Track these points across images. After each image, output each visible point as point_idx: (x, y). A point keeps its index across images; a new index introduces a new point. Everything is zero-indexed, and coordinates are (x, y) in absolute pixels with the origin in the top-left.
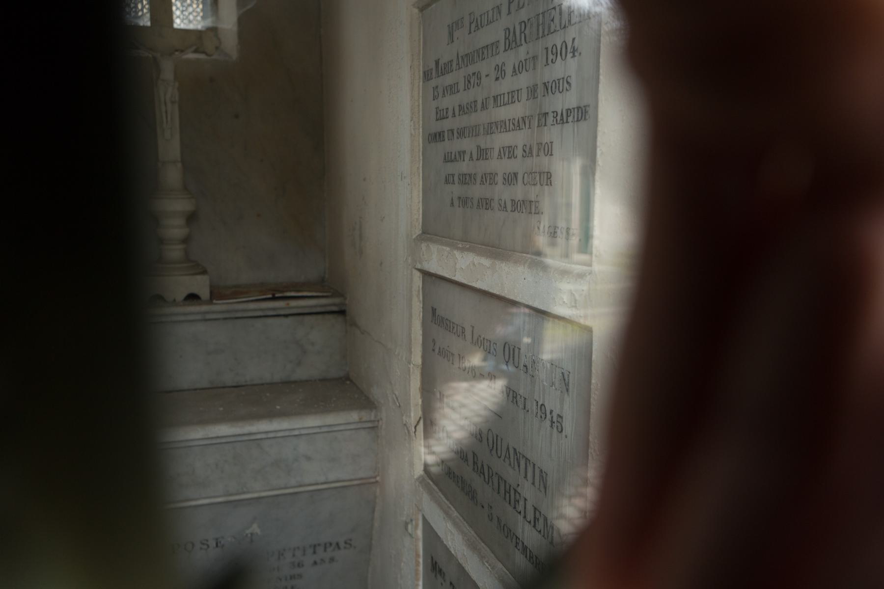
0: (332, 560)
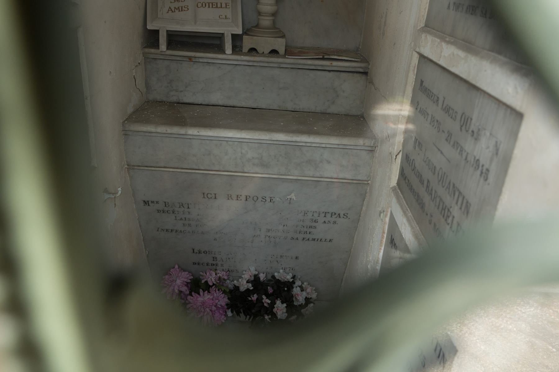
0: (335, 222)
